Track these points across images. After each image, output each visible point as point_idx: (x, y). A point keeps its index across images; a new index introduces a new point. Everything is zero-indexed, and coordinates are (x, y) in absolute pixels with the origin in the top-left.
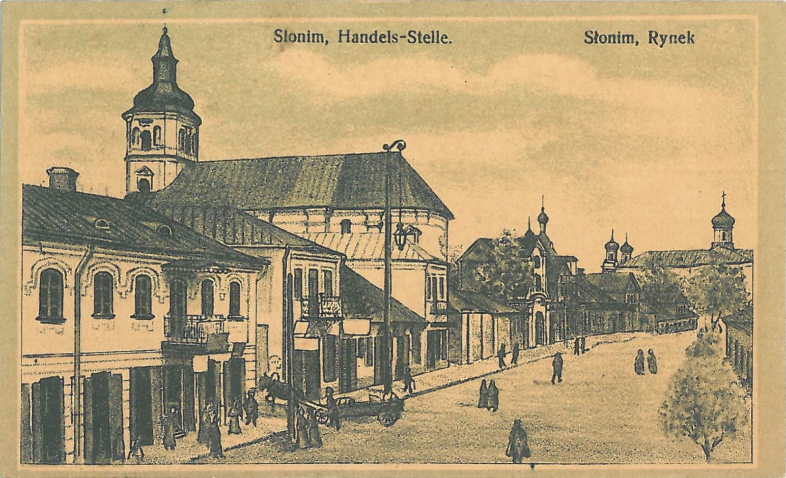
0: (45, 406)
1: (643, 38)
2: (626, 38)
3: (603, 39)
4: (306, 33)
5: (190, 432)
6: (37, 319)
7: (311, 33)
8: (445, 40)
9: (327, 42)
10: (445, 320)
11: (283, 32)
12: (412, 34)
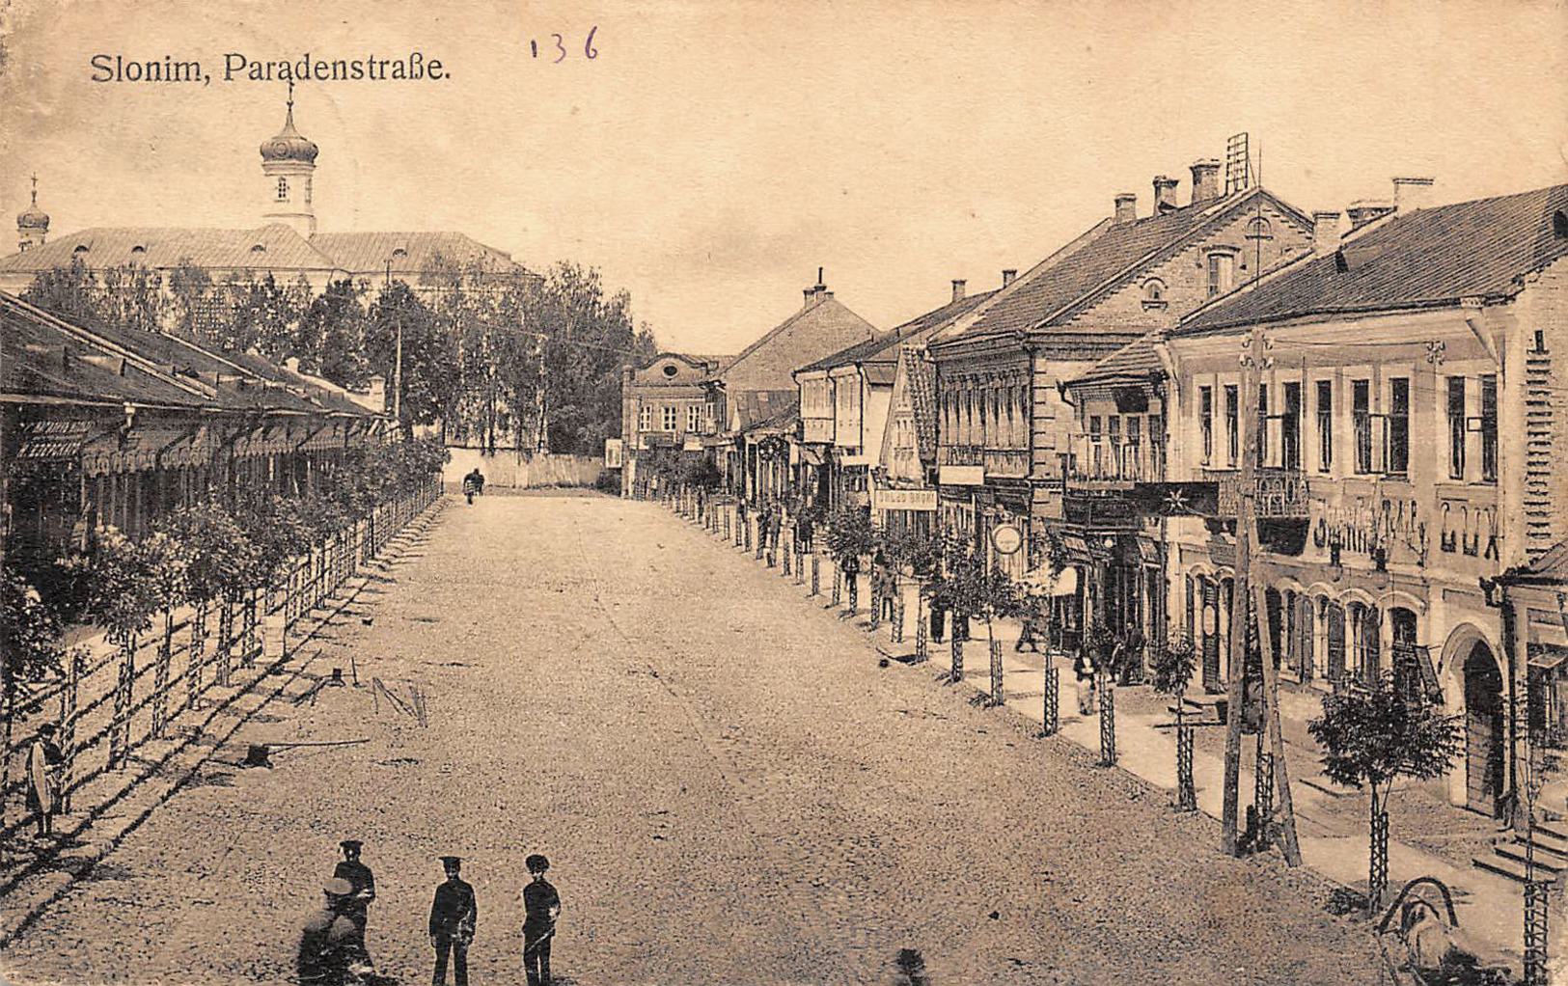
2: (183, 69)
4: (163, 63)
12: (100, 61)
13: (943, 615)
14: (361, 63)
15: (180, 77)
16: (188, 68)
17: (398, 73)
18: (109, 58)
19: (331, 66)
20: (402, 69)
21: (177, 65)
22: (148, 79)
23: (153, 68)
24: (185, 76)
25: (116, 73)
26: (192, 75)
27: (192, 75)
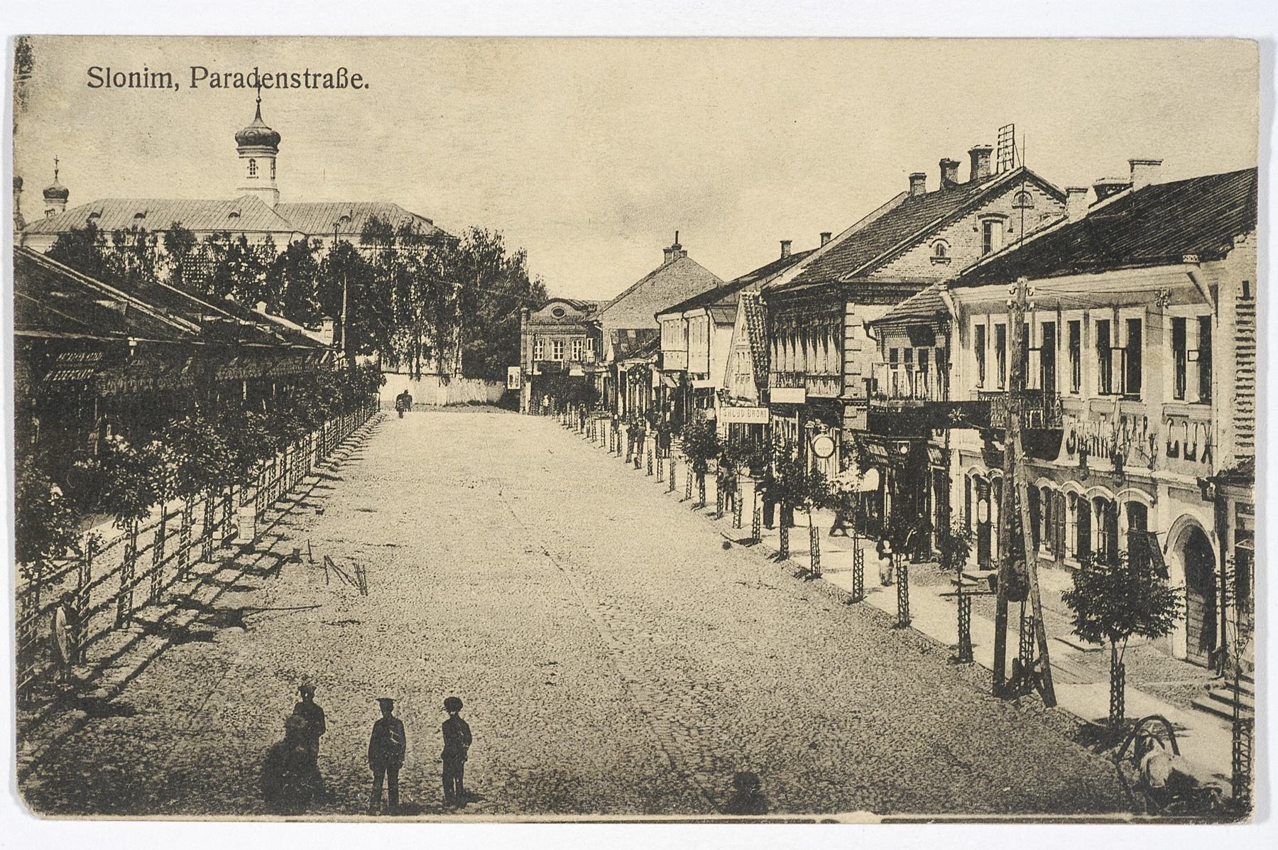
0: (1039, 501)
1: (183, 79)
2: (158, 78)
3: (120, 80)
4: (142, 72)
5: (179, 529)
6: (406, 392)
7: (149, 72)
8: (357, 83)
9: (177, 85)
10: (1094, 548)
11: (105, 71)
12: (94, 72)
14: (299, 76)
18: (101, 70)
21: (153, 75)
23: (282, 78)
24: (312, 85)
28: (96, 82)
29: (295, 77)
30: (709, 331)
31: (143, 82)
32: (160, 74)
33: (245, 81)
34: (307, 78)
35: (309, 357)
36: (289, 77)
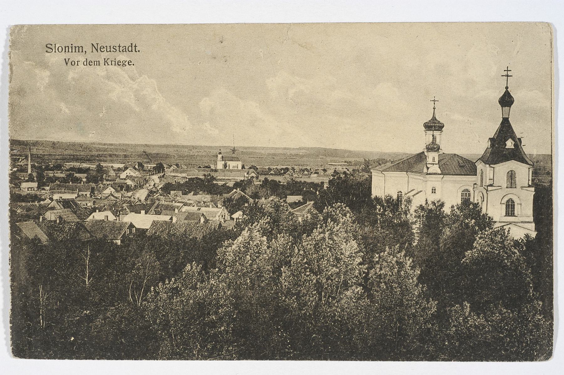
2: (77, 49)
4: (70, 46)
12: (49, 46)
13: (300, 195)
14: (116, 47)
15: (109, 47)
16: (79, 48)
17: (124, 50)
18: (52, 45)
19: (93, 62)
20: (126, 49)
21: (75, 47)
22: (65, 52)
23: (67, 48)
24: (71, 51)
25: (54, 50)
26: (81, 50)
27: (81, 50)
28: (49, 50)
29: (114, 47)
30: (498, 186)
31: (70, 50)
32: (78, 47)
33: (127, 50)
34: (119, 48)
35: (41, 321)
36: (112, 47)
